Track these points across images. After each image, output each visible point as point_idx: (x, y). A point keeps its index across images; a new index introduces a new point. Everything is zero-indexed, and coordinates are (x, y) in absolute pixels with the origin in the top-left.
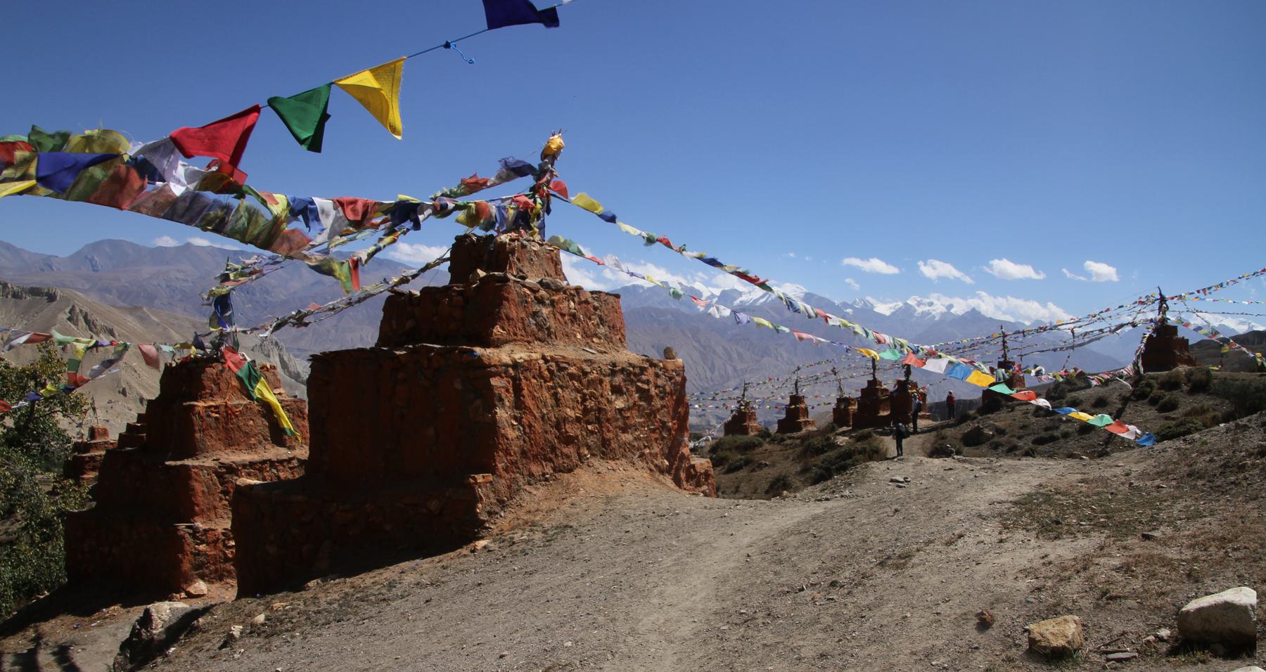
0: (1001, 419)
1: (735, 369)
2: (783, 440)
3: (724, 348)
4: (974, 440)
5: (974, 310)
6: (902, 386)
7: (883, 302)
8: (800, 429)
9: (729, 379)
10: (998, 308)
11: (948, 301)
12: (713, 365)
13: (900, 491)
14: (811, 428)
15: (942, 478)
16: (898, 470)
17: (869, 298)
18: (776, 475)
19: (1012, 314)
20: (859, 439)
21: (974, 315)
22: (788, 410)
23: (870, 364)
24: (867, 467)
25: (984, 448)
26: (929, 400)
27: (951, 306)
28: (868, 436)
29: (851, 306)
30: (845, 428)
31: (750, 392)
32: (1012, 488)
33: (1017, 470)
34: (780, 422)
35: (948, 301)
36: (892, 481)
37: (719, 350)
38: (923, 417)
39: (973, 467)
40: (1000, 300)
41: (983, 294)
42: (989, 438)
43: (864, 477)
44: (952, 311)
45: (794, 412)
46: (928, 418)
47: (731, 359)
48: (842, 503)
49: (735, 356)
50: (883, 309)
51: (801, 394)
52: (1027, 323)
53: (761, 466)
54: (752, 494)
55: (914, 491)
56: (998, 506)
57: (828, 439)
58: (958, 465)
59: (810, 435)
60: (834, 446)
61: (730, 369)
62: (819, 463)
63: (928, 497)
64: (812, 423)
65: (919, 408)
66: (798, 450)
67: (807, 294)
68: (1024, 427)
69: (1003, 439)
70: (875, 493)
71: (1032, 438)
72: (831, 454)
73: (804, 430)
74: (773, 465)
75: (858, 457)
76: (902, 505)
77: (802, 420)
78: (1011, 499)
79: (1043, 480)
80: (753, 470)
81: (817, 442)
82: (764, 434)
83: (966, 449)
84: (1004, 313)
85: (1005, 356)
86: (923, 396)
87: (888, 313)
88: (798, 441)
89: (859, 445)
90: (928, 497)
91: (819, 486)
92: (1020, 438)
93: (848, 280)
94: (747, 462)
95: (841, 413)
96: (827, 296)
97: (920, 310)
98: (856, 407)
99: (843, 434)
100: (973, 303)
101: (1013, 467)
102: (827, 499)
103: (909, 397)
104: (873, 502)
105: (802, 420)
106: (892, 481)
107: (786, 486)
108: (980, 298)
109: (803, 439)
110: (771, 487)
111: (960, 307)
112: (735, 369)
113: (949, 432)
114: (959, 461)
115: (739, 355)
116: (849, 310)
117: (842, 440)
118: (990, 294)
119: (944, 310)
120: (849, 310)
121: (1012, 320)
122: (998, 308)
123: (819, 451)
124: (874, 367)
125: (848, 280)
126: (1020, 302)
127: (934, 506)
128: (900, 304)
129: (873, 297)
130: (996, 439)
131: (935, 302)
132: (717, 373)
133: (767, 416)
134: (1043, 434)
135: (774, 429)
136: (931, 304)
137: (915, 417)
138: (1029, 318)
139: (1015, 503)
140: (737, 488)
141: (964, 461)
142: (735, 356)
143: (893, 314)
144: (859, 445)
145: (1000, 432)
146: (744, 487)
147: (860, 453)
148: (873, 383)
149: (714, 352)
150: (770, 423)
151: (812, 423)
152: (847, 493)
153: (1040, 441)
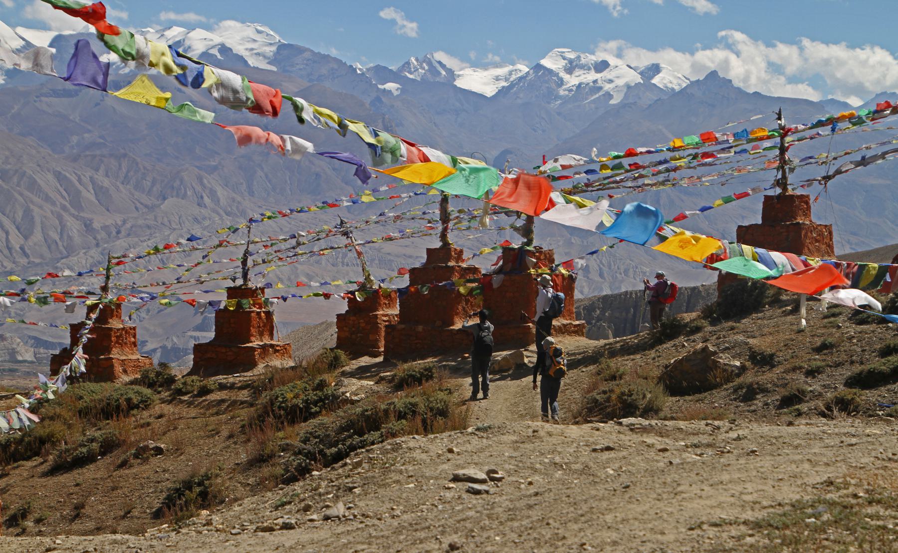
0: (759, 331)
1: (88, 226)
2: (204, 391)
3: (58, 176)
4: (691, 380)
5: (713, 74)
6: (514, 260)
7: (479, 64)
8: (253, 365)
9: (71, 250)
10: (775, 68)
11: (646, 59)
12: (28, 213)
13: (474, 500)
14: (277, 362)
15: (586, 470)
16: (468, 452)
17: (440, 56)
18: (183, 476)
19: (815, 81)
20: (400, 385)
21: (715, 84)
22: (222, 316)
23: (436, 212)
24: (396, 448)
25: (718, 398)
26: (582, 292)
27: (656, 69)
28: (427, 375)
29: (395, 76)
30: (365, 361)
31: (122, 278)
32: (751, 490)
33: (775, 445)
34: (199, 349)
35: (646, 59)
36: (456, 479)
37: (47, 181)
38: (564, 330)
39: (668, 442)
40: (784, 51)
41: (739, 36)
42: (730, 375)
43: (386, 470)
44: (656, 81)
45: (236, 329)
46: (578, 331)
47: (77, 202)
48: (324, 533)
49: (89, 195)
50: (478, 81)
51: (255, 283)
52: (855, 102)
53: (142, 454)
54: (125, 518)
55: (503, 501)
56: (712, 532)
57: (322, 385)
58: (629, 438)
59: (274, 378)
60: (333, 402)
61: (74, 227)
62: (296, 443)
63: (536, 514)
64: (283, 351)
65: (556, 308)
66: (244, 414)
67: (281, 47)
68: (824, 348)
69: (767, 377)
70: (411, 508)
71: (848, 372)
72: (329, 421)
73: (260, 368)
74: (178, 449)
75: (394, 424)
76: (470, 534)
77: (255, 343)
78: (749, 515)
79: (837, 472)
80: (124, 464)
81: (292, 394)
82: (158, 380)
83: (669, 402)
84: (793, 80)
85: (782, 183)
86: (568, 284)
87: (490, 91)
88: (244, 395)
89: (400, 400)
90: (536, 514)
91: (272, 497)
92: (812, 373)
93: (387, 14)
94: (108, 447)
95: (357, 325)
96: (334, 53)
97: (572, 81)
98: (396, 311)
99: (361, 373)
100: (710, 58)
101: (769, 441)
102: (287, 527)
103: (530, 287)
104: (398, 531)
105: (255, 343)
106: (456, 479)
107: (208, 498)
108: (730, 46)
109: (255, 388)
110: (169, 502)
111: (676, 70)
112: (88, 226)
113: (625, 364)
114: (632, 428)
115: (99, 191)
116: (391, 86)
117: (354, 388)
118: (754, 37)
119: (635, 78)
120: (391, 86)
121: (813, 96)
122: (775, 68)
123: (296, 414)
124: (445, 218)
125: (387, 14)
126: (838, 52)
127: (547, 533)
128: (524, 69)
129: (450, 52)
130: (749, 378)
131: (612, 61)
132: (38, 236)
133: (167, 334)
134: (878, 364)
135: (181, 367)
136: (602, 66)
137: (545, 326)
138: (858, 89)
139: (757, 526)
140: (79, 507)
141: (645, 430)
142: (89, 195)
143: (502, 92)
144: (400, 400)
145: (763, 360)
146: (95, 505)
147: (401, 416)
148: (441, 256)
149: (33, 186)
150: (177, 352)
151: (283, 351)
152: (339, 509)
153: (868, 380)
